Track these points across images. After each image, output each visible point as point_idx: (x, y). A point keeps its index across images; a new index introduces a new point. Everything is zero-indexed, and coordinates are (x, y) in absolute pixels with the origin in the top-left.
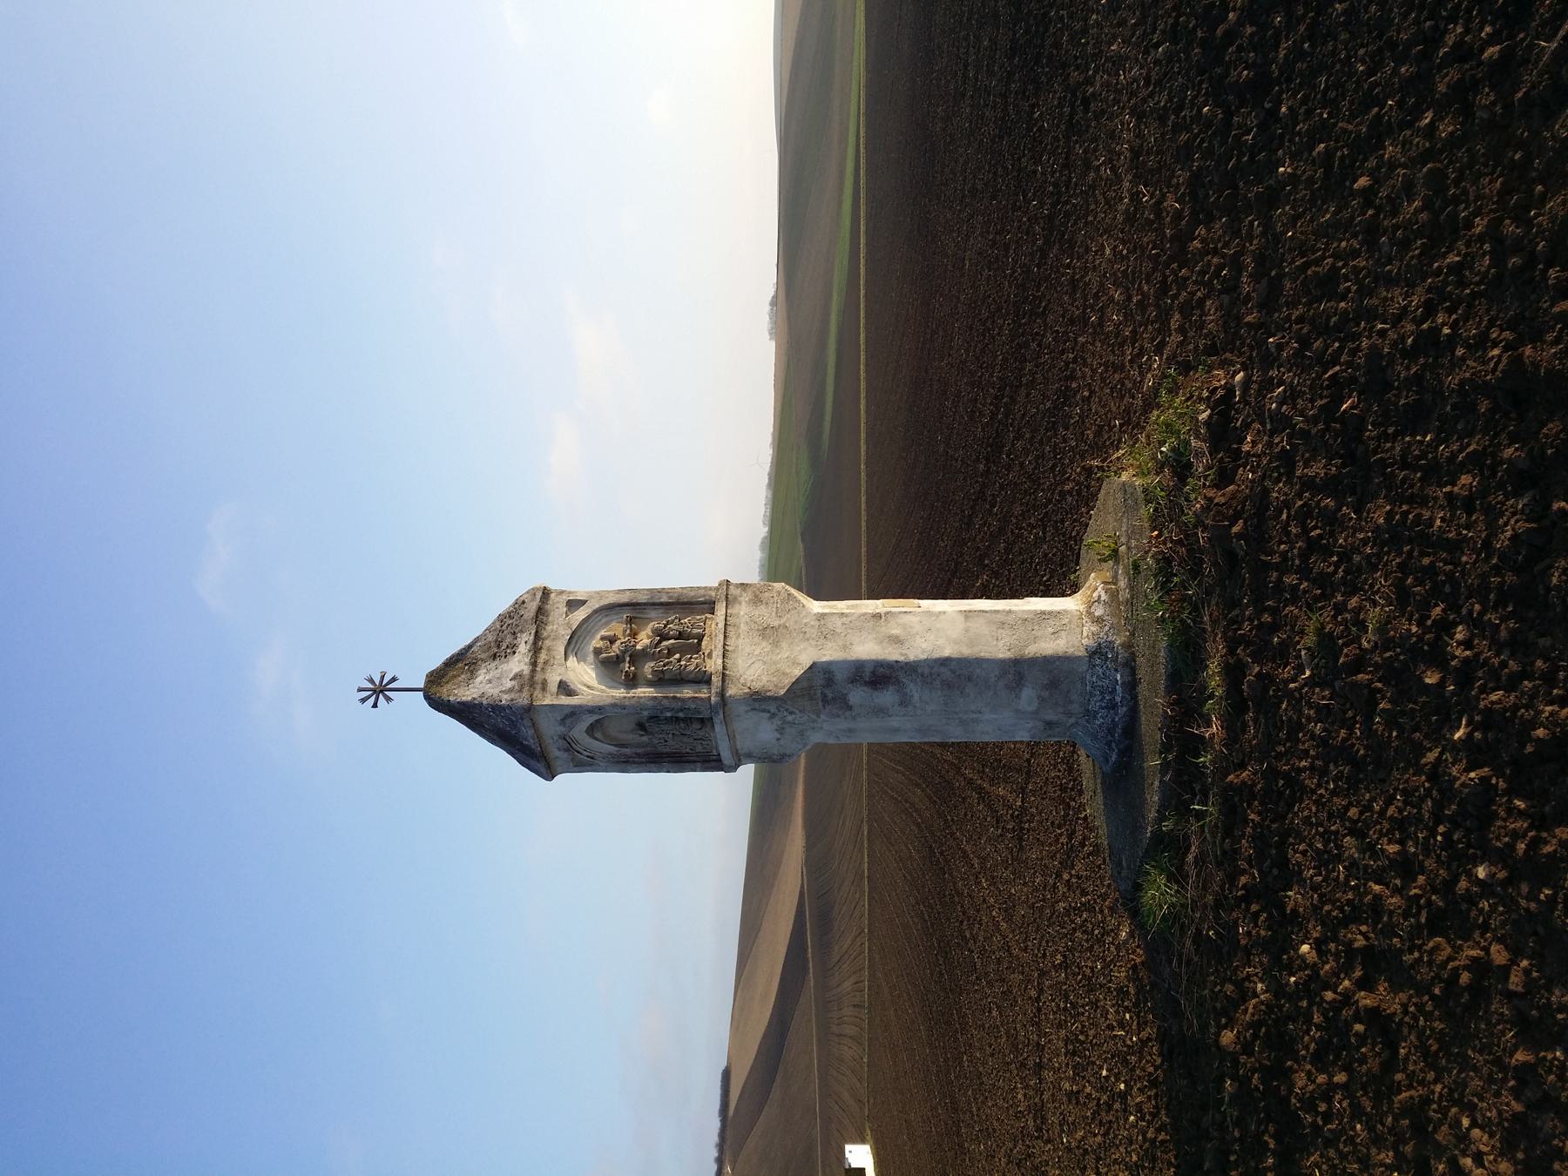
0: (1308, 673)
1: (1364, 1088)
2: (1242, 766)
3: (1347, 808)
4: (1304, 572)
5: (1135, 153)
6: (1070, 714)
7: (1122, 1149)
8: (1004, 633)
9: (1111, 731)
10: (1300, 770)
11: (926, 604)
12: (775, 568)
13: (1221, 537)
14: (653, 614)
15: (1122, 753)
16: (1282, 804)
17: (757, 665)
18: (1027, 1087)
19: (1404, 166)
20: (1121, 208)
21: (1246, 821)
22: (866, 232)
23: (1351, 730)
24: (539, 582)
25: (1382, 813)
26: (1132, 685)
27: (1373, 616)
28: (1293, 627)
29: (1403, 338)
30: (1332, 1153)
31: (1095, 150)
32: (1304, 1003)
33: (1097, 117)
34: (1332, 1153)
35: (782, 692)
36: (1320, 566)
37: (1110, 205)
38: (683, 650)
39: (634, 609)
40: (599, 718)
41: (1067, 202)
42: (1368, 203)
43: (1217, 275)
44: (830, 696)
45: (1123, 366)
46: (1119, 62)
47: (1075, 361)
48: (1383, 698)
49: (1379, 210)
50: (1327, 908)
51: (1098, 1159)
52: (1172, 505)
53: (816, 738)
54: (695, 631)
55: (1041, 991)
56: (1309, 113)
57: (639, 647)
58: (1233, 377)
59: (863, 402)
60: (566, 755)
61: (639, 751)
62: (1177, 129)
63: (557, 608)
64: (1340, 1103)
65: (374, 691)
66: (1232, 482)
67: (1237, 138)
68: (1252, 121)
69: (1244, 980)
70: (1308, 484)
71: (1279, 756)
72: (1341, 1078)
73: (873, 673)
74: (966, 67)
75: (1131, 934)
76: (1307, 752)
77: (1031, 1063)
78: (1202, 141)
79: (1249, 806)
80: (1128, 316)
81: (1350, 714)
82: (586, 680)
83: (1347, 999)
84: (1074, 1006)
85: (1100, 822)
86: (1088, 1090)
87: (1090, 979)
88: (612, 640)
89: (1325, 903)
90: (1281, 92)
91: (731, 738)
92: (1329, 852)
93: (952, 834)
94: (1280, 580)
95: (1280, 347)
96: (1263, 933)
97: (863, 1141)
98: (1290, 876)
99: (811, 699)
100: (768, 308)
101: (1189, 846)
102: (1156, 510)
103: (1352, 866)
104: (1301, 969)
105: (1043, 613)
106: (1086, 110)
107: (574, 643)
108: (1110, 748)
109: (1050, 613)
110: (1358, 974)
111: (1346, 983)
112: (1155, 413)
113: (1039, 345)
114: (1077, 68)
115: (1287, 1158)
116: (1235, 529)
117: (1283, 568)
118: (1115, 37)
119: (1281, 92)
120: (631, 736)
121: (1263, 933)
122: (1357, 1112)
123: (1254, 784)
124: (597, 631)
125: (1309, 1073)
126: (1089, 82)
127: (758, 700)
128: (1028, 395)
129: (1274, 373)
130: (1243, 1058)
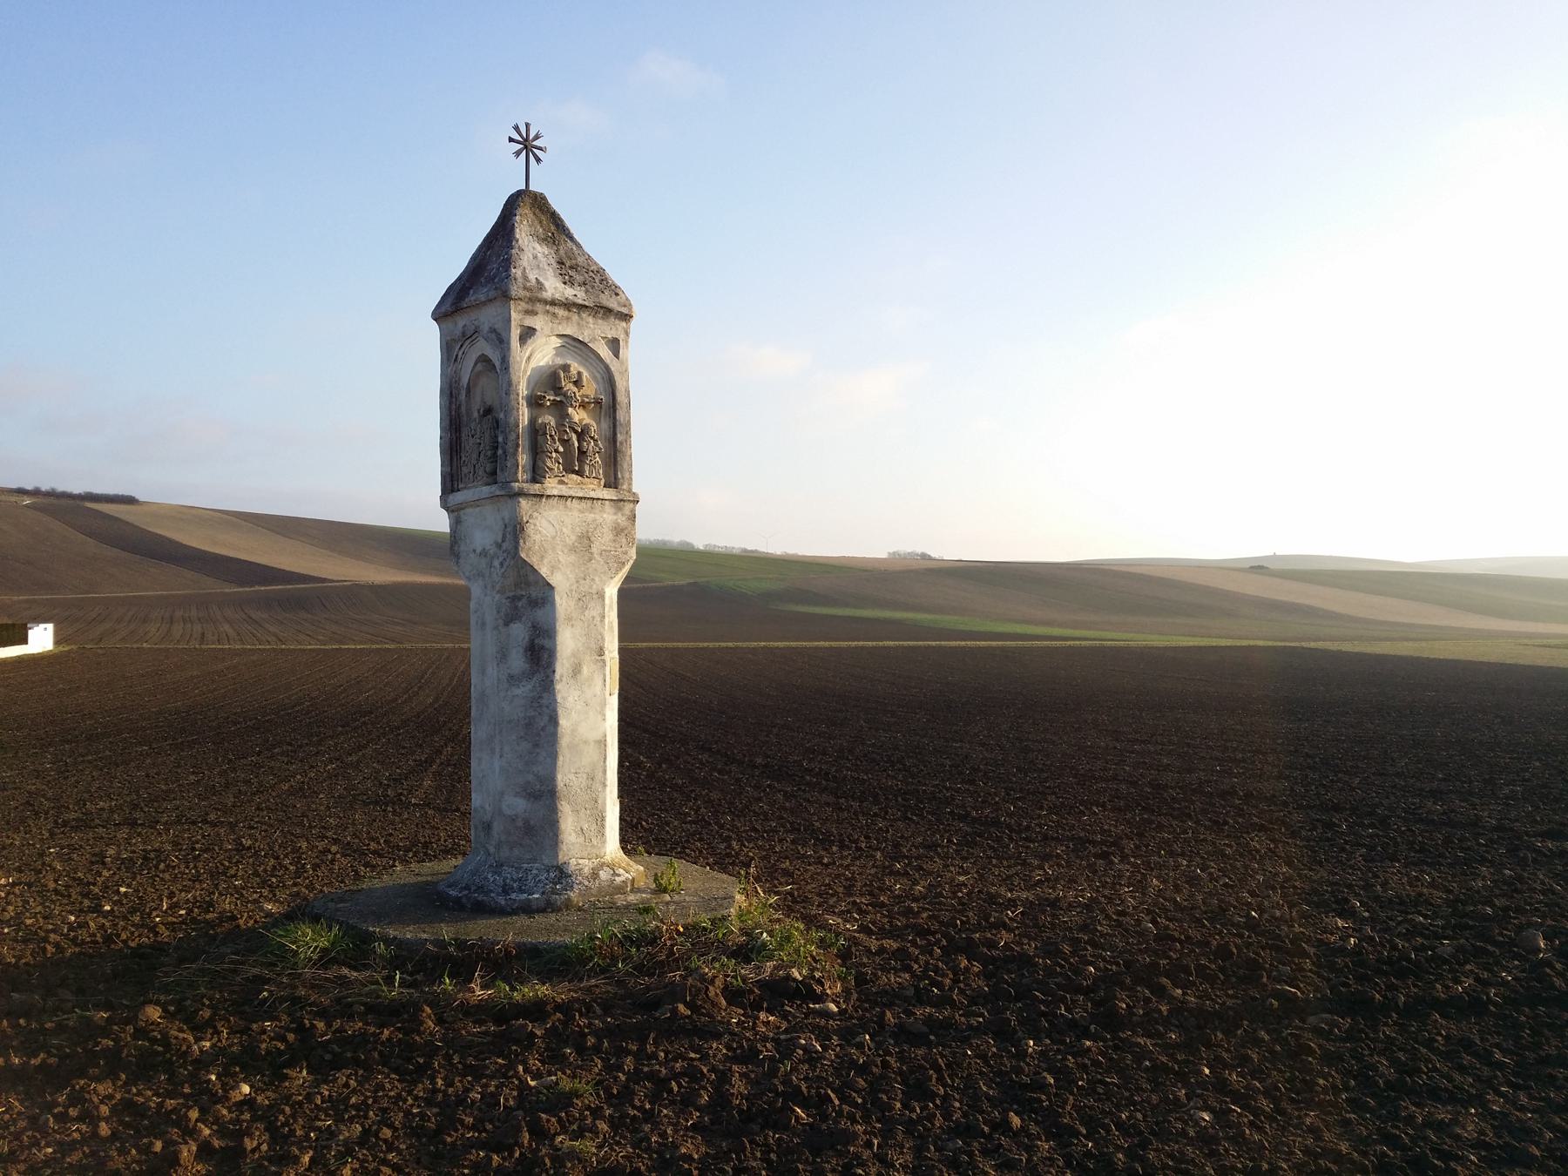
0: (532, 1083)
1: (93, 1154)
2: (440, 1021)
3: (391, 1126)
4: (635, 1077)
5: (1054, 904)
6: (498, 846)
7: (39, 909)
8: (582, 780)
9: (480, 889)
10: (433, 1079)
11: (613, 703)
12: (651, 556)
13: (675, 993)
14: (605, 425)
15: (458, 900)
16: (399, 1061)
18: (112, 811)
19: (1029, 1160)
20: (1002, 890)
21: (382, 1026)
23: (473, 1128)
24: (636, 311)
25: (385, 1162)
26: (528, 910)
27: (588, 1146)
28: (580, 1067)
29: (862, 1165)
30: (22, 1124)
31: (1059, 865)
32: (187, 1090)
33: (1091, 866)
34: (22, 1124)
35: (523, 555)
36: (641, 1092)
37: (1006, 881)
38: (567, 455)
39: (610, 406)
40: (496, 368)
41: (1011, 839)
42: (995, 1127)
43: (934, 983)
45: (851, 895)
46: (1141, 886)
47: (859, 849)
48: (504, 1159)
49: (989, 1137)
50: (287, 1109)
51: (30, 885)
52: (708, 945)
53: (476, 590)
54: (587, 468)
55: (214, 825)
56: (1084, 1067)
57: (570, 410)
58: (834, 1001)
59: (827, 644)
61: (463, 409)
62: (1075, 942)
63: (612, 329)
64: (77, 1130)
65: (526, 140)
66: (729, 1003)
67: (1063, 1000)
68: (1079, 1014)
69: (215, 1027)
70: (724, 1077)
71: (448, 1058)
72: (104, 1130)
73: (543, 647)
74: (1143, 742)
75: (269, 914)
76: (451, 1085)
77: (137, 815)
78: (1062, 967)
79: (399, 1029)
80: (899, 899)
81: (489, 1127)
82: (536, 355)
83: (189, 1132)
84: (196, 858)
86: (106, 873)
87: (224, 874)
89: (292, 1107)
90: (1104, 1040)
91: (476, 503)
92: (346, 1110)
93: (384, 734)
94: (628, 1052)
95: (860, 1046)
96: (264, 1046)
97: (57, 642)
98: (322, 1071)
99: (516, 585)
100: (919, 550)
101: (355, 969)
102: (705, 929)
103: (331, 1134)
104: (224, 1085)
105: (603, 819)
106: (1097, 856)
107: (575, 345)
108: (462, 889)
109: (603, 826)
110: (216, 1143)
111: (207, 1132)
112: (802, 927)
113: (875, 815)
114: (1137, 847)
115: (15, 1078)
116: (681, 1007)
117: (641, 1056)
118: (1164, 882)
119: (1104, 1040)
120: (478, 399)
121: (264, 1046)
122: (65, 1148)
123: (419, 1033)
125: (110, 1097)
126: (1124, 858)
127: (515, 531)
128: (828, 804)
129: (835, 1040)
130: (130, 1029)
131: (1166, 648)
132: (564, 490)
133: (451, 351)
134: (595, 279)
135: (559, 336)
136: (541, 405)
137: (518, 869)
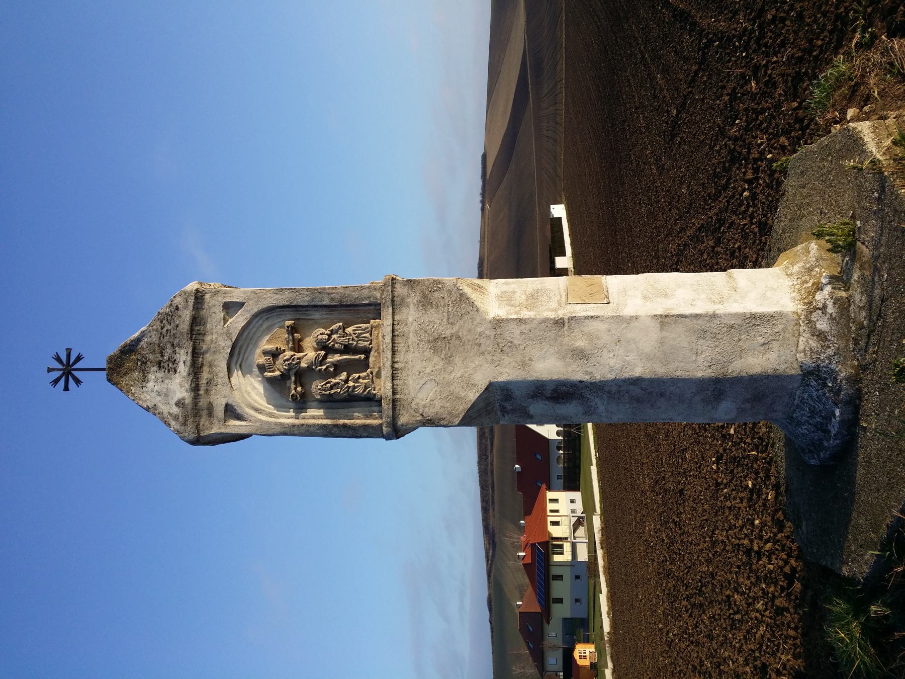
17: (428, 386)
26: (852, 425)
39: (298, 314)
54: (362, 344)
105: (753, 316)
107: (237, 355)
124: (256, 345)
132: (386, 373)
135: (230, 375)
136: (303, 395)
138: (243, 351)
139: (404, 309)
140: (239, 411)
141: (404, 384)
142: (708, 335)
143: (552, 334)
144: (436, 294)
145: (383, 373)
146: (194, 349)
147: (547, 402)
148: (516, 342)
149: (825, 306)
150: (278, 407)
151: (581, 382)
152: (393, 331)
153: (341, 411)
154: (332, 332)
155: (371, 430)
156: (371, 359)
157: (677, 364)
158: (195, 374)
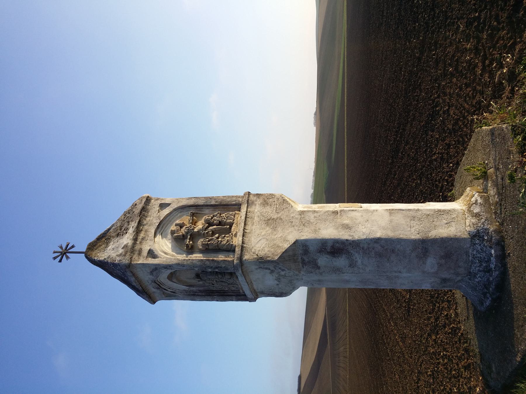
6: (458, 274)
9: (486, 286)
11: (365, 206)
14: (207, 211)
17: (262, 241)
22: (347, 88)
26: (502, 257)
35: (276, 258)
39: (195, 209)
40: (174, 271)
44: (307, 260)
54: (229, 221)
57: (196, 230)
60: (158, 291)
63: (154, 206)
65: (61, 253)
73: (332, 247)
82: (164, 249)
85: (473, 336)
88: (181, 226)
100: (313, 116)
105: (439, 211)
107: (160, 228)
124: (175, 220)
127: (262, 262)
131: (347, 24)
132: (240, 234)
133: (171, 295)
134: (127, 217)
135: (155, 236)
136: (192, 247)
137: (472, 262)
138: (164, 227)
139: (253, 207)
140: (156, 253)
141: (249, 240)
142: (416, 219)
143: (331, 217)
144: (271, 200)
145: (238, 234)
146: (139, 221)
147: (328, 256)
148: (311, 221)
149: (476, 201)
150: (177, 253)
151: (347, 240)
152: (246, 214)
153: (212, 255)
154: (214, 216)
155: (227, 263)
156: (233, 228)
157: (400, 232)
158: (137, 232)
